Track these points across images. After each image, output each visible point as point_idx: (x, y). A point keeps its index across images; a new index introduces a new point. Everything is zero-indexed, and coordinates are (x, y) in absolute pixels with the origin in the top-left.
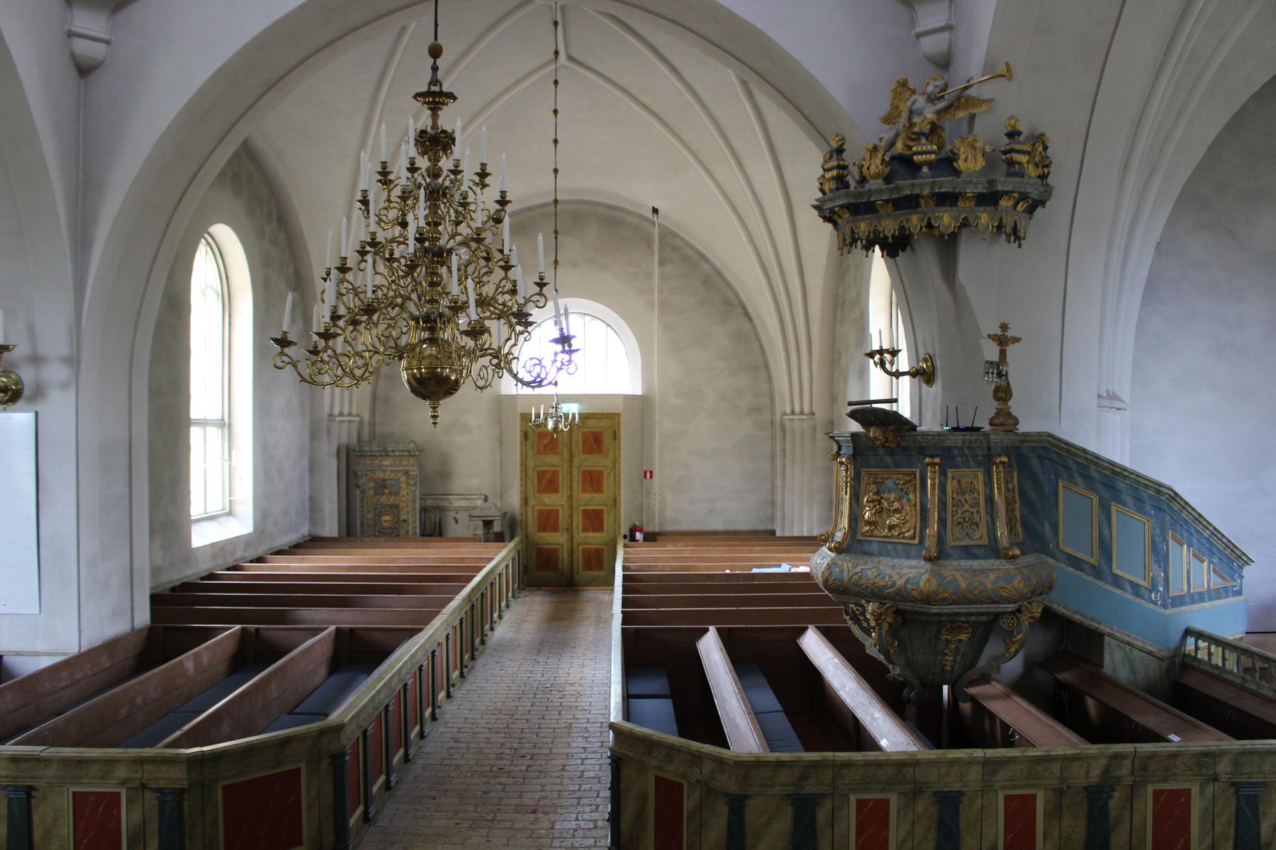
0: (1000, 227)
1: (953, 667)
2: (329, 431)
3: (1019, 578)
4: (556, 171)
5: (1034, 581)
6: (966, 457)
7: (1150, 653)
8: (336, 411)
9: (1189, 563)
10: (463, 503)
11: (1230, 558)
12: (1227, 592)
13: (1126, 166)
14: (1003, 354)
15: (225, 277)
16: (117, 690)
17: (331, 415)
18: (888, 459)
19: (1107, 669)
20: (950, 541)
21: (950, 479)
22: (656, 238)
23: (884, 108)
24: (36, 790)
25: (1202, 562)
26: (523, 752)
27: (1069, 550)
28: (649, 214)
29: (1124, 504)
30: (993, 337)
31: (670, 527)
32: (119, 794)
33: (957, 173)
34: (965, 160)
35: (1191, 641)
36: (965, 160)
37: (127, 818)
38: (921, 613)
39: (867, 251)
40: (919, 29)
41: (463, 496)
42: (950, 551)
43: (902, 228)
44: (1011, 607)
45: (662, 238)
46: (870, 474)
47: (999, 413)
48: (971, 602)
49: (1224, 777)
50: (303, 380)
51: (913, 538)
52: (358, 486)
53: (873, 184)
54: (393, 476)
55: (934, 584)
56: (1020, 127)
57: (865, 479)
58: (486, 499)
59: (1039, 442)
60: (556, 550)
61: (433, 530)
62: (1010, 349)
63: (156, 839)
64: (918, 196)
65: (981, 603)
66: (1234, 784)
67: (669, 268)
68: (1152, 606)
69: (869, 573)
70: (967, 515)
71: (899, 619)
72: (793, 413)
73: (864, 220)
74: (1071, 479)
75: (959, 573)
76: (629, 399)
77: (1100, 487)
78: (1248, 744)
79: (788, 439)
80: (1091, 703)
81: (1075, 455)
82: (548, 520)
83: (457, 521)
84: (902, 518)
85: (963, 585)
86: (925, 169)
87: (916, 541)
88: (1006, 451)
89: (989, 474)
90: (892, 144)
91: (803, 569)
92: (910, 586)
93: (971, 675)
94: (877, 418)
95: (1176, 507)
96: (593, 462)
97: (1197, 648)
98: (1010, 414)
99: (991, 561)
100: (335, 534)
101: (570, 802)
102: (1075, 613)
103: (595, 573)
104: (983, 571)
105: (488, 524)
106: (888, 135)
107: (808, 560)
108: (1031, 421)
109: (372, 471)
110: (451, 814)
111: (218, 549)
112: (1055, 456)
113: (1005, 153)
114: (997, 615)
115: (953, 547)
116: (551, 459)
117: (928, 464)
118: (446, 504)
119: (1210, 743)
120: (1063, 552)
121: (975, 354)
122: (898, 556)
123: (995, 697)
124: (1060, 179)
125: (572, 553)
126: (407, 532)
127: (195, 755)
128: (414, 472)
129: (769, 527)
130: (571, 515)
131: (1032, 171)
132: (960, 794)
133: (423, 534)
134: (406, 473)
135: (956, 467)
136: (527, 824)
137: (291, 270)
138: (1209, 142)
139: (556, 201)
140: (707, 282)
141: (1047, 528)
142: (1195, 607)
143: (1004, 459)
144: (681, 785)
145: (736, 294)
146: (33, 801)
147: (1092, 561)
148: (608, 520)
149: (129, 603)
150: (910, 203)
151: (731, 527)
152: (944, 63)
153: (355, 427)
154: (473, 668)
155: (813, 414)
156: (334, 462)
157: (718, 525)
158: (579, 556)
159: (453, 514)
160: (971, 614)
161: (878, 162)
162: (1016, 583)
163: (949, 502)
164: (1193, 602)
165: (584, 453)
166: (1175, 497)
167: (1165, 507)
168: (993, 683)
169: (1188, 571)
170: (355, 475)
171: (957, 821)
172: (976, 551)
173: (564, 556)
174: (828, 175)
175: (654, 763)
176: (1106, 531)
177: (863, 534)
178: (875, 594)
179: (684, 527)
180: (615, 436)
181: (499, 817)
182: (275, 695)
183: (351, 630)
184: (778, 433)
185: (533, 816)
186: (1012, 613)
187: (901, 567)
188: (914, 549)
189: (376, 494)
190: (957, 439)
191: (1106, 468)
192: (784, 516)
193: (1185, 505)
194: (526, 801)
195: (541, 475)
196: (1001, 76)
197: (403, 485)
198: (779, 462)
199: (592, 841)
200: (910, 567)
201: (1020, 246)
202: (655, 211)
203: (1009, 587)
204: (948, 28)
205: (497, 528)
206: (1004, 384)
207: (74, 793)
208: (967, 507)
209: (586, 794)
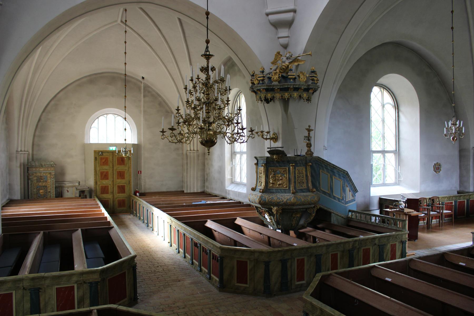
2: (16, 158)
4: (125, 64)
7: (342, 217)
8: (19, 150)
10: (70, 185)
14: (309, 134)
17: (17, 151)
18: (277, 165)
19: (332, 222)
22: (142, 88)
23: (272, 59)
27: (323, 189)
28: (141, 79)
30: (307, 129)
40: (279, 36)
41: (71, 182)
46: (272, 169)
47: (308, 151)
48: (304, 205)
49: (377, 244)
50: (176, 143)
51: (287, 187)
53: (274, 83)
54: (44, 175)
55: (295, 200)
60: (108, 201)
66: (379, 245)
72: (190, 150)
74: (323, 170)
76: (134, 145)
79: (189, 159)
83: (68, 192)
84: (282, 181)
85: (303, 200)
86: (292, 80)
89: (306, 168)
92: (288, 201)
97: (352, 215)
100: (19, 198)
103: (122, 208)
104: (307, 196)
109: (36, 173)
114: (307, 209)
116: (106, 168)
124: (319, 84)
125: (114, 201)
126: (51, 196)
129: (182, 190)
130: (113, 188)
132: (321, 255)
133: (56, 197)
139: (125, 74)
140: (160, 104)
143: (310, 164)
144: (247, 262)
148: (127, 189)
150: (286, 89)
152: (285, 47)
153: (26, 155)
155: (198, 150)
156: (19, 170)
157: (164, 189)
159: (66, 189)
165: (118, 165)
178: (277, 204)
179: (152, 191)
189: (37, 182)
195: (102, 173)
197: (49, 178)
198: (185, 167)
202: (143, 78)
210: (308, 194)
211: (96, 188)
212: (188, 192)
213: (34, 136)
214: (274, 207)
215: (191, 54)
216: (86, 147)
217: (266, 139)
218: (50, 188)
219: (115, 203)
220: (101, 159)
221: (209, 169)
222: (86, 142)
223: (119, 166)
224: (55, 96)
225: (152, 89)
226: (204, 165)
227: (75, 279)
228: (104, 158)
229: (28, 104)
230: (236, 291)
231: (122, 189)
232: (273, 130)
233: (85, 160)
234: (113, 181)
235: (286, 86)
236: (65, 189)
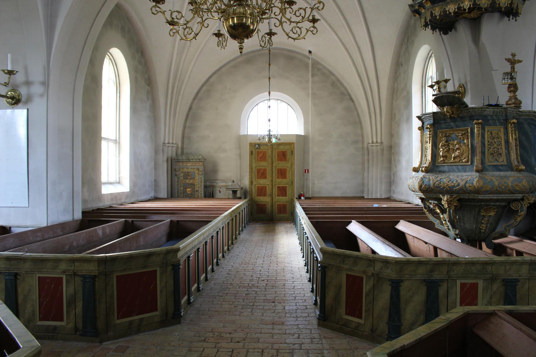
1: (485, 231)
6: (494, 120)
8: (166, 142)
14: (513, 68)
15: (118, 75)
16: (64, 236)
17: (164, 143)
18: (452, 124)
20: (487, 163)
22: (310, 65)
24: (20, 275)
26: (263, 279)
30: (508, 60)
31: (316, 195)
32: (62, 278)
37: (66, 291)
41: (224, 181)
43: (459, 8)
45: (313, 65)
46: (442, 133)
52: (176, 175)
54: (192, 170)
55: (481, 184)
58: (233, 182)
60: (265, 205)
61: (209, 194)
62: (517, 66)
63: (81, 302)
65: (505, 194)
67: (316, 79)
69: (445, 180)
70: (496, 149)
72: (373, 143)
73: (437, 6)
75: (496, 178)
76: (298, 136)
82: (262, 191)
83: (220, 192)
85: (497, 183)
87: (469, 163)
93: (493, 235)
96: (282, 165)
98: (517, 99)
99: (510, 172)
101: (291, 298)
103: (283, 215)
104: (506, 177)
105: (234, 192)
109: (182, 168)
110: (231, 303)
111: (114, 196)
115: (489, 166)
116: (263, 164)
118: (216, 184)
122: (459, 171)
125: (272, 206)
126: (198, 196)
127: (102, 257)
128: (201, 168)
129: (361, 195)
130: (272, 189)
132: (517, 280)
134: (198, 169)
135: (490, 125)
136: (271, 307)
137: (147, 76)
140: (333, 84)
143: (515, 121)
145: (346, 89)
146: (18, 281)
149: (71, 207)
151: (343, 195)
153: (174, 149)
154: (232, 248)
155: (382, 143)
156: (165, 164)
158: (275, 208)
159: (218, 189)
162: (524, 183)
163: (486, 143)
170: (175, 170)
171: (516, 295)
172: (501, 168)
173: (269, 207)
175: (346, 267)
178: (449, 191)
179: (322, 195)
180: (292, 153)
181: (256, 304)
182: (142, 243)
183: (178, 221)
184: (366, 153)
185: (273, 304)
188: (468, 168)
189: (184, 179)
190: (490, 111)
192: (368, 189)
194: (268, 297)
195: (258, 171)
197: (196, 175)
198: (366, 165)
199: (307, 315)
200: (467, 176)
201: (516, 20)
202: (310, 52)
203: (520, 185)
205: (238, 195)
207: (39, 277)
208: (495, 145)
209: (298, 295)
210: (508, 173)
211: (251, 188)
212: (369, 197)
213: (185, 127)
214: (444, 196)
215: (365, 11)
216: (241, 139)
218: (197, 186)
219: (274, 207)
220: (258, 153)
221: (396, 167)
222: (243, 132)
223: (279, 162)
224: (208, 80)
225: (322, 65)
226: (390, 161)
227: (63, 266)
228: (261, 152)
229: (175, 90)
230: (344, 329)
231: (282, 191)
232: (459, 80)
233: (240, 155)
234: (272, 180)
236: (216, 188)
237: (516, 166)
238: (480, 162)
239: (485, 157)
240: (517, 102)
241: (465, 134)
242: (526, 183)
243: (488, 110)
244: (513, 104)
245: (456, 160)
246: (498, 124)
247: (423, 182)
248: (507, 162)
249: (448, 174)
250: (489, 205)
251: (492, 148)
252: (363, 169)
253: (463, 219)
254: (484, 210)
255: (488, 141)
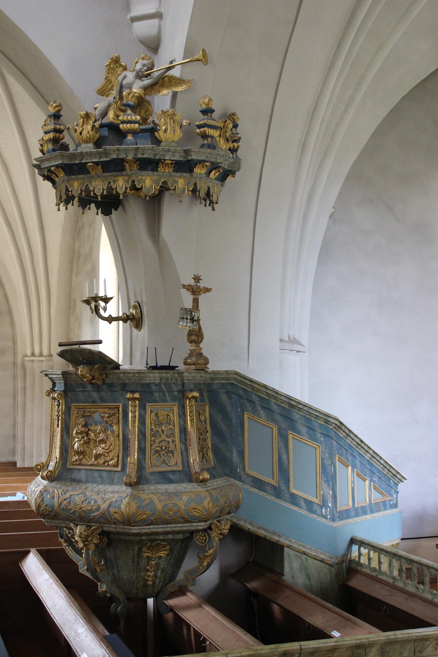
0: (194, 191)
1: (154, 583)
3: (208, 499)
5: (222, 502)
6: (163, 392)
7: (322, 561)
9: (353, 482)
11: (388, 477)
12: (385, 506)
13: (304, 146)
14: (196, 302)
18: (95, 394)
20: (149, 469)
21: (148, 412)
23: (100, 82)
25: (364, 480)
27: (253, 473)
29: (299, 433)
30: (188, 288)
33: (158, 142)
34: (165, 131)
35: (355, 548)
36: (165, 131)
38: (124, 534)
39: (84, 207)
40: (134, 14)
42: (149, 477)
43: (110, 189)
44: (202, 525)
46: (78, 408)
56: (213, 106)
57: (74, 412)
59: (228, 379)
62: (202, 298)
64: (123, 160)
65: (176, 523)
68: (323, 520)
69: (77, 498)
71: (105, 540)
72: (33, 355)
73: (77, 179)
74: (255, 412)
77: (278, 418)
78: (391, 635)
80: (276, 608)
81: (259, 390)
85: (159, 507)
87: (119, 469)
88: (198, 387)
89: (183, 407)
90: (104, 114)
91: (19, 497)
92: (112, 510)
93: (171, 588)
94: (83, 358)
95: (342, 434)
97: (360, 554)
98: (201, 354)
99: (185, 485)
102: (260, 528)
104: (177, 494)
106: (101, 105)
107: (25, 489)
108: (219, 363)
112: (241, 392)
113: (199, 127)
114: (192, 533)
115: (152, 473)
117: (129, 399)
119: (362, 637)
120: (248, 475)
121: (173, 302)
122: (103, 483)
123: (188, 607)
124: (248, 152)
129: (11, 459)
131: (223, 145)
135: (155, 401)
138: (372, 130)
141: (235, 454)
142: (358, 519)
147: (273, 483)
150: (116, 166)
160: (168, 533)
161: (89, 127)
163: (148, 433)
164: (357, 515)
166: (340, 426)
167: (332, 434)
168: (189, 594)
169: (353, 489)
172: (171, 476)
174: (47, 137)
176: (284, 457)
177: (73, 464)
178: (83, 518)
186: (204, 530)
187: (105, 492)
190: (155, 376)
191: (283, 402)
192: (24, 449)
193: (349, 433)
196: (198, 60)
200: (113, 492)
203: (200, 508)
204: (158, 15)
206: (196, 328)
208: (163, 437)
217: (110, 319)
235: (114, 156)
237: (196, 473)
238: (136, 467)
239: (145, 458)
240: (201, 361)
241: (114, 414)
242: (210, 505)
243: (151, 375)
244: (194, 364)
245: (101, 461)
246: (168, 398)
247: (42, 500)
248: (183, 465)
249: (84, 487)
250: (157, 540)
251: (157, 441)
252: (15, 407)
253: (116, 563)
254: (148, 548)
255: (151, 429)
